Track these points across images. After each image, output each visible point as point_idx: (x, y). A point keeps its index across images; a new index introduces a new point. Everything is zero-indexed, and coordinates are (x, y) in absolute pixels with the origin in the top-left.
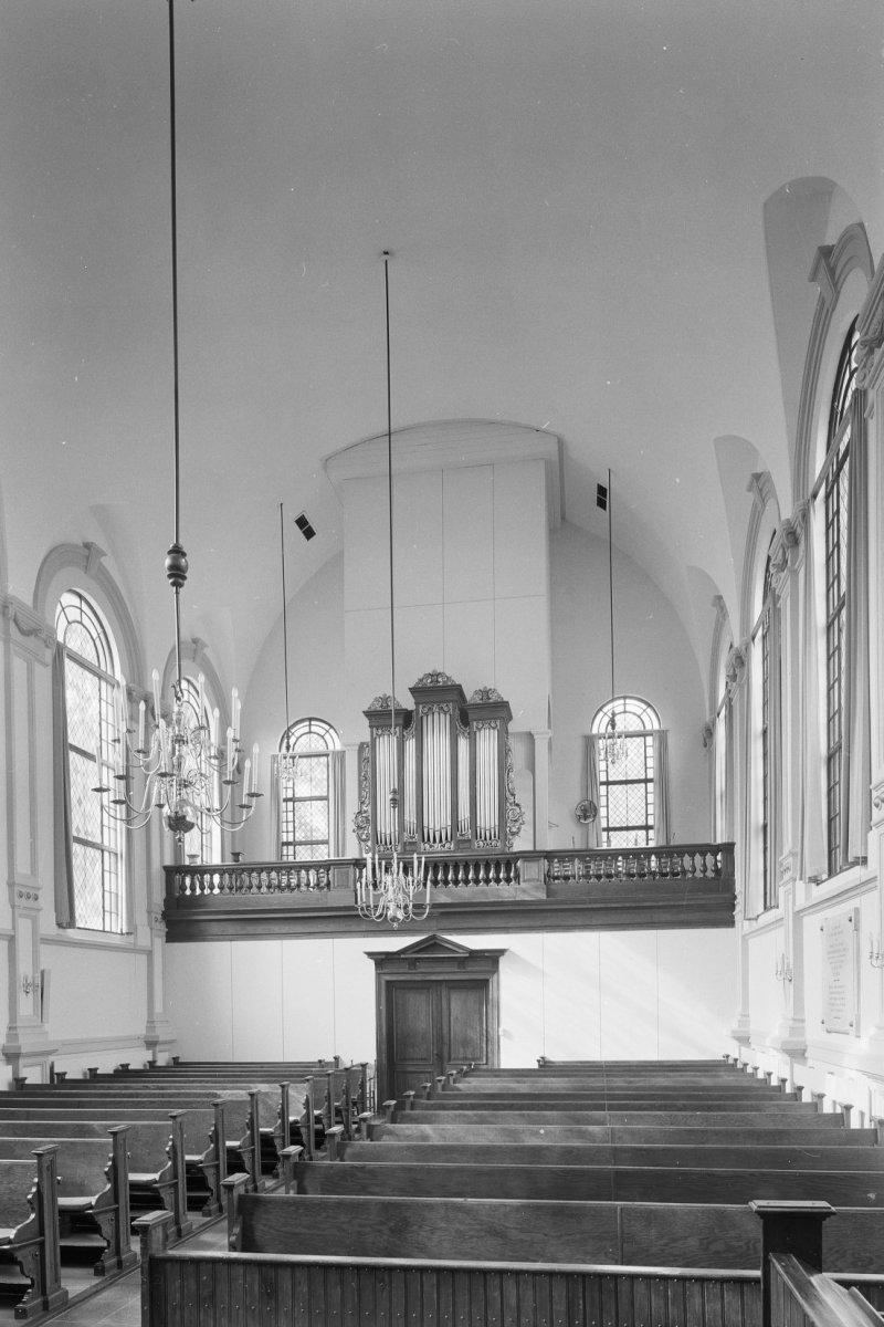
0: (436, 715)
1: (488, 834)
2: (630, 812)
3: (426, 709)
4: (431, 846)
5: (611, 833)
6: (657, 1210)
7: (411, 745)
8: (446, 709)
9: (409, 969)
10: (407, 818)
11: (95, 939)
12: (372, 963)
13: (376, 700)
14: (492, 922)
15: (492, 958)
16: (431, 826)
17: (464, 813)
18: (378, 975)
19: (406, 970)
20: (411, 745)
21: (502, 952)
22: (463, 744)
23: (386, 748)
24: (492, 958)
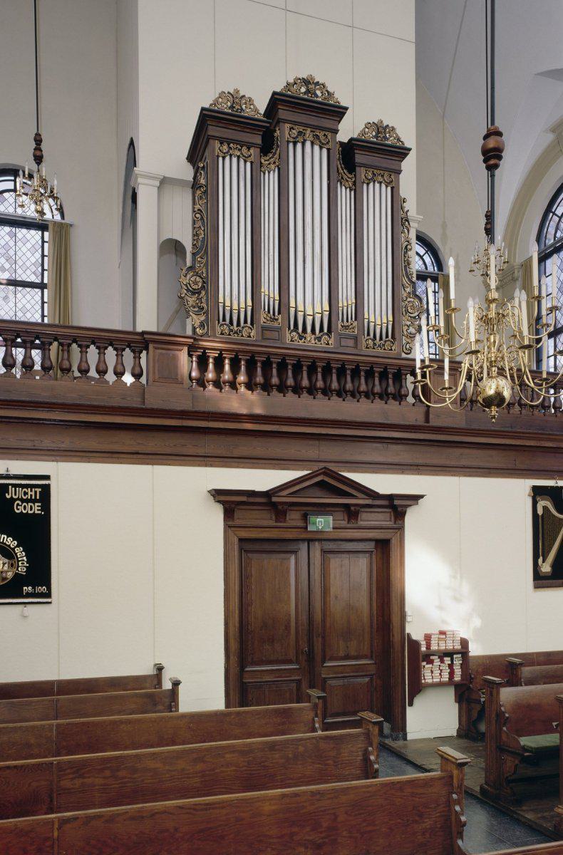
0: (308, 144)
1: (309, 319)
2: (20, 244)
3: (295, 132)
4: (301, 337)
5: (38, 281)
6: (287, 793)
7: (271, 181)
8: (322, 138)
9: (349, 522)
10: (264, 289)
11: (282, 536)
12: (216, 515)
13: (368, 125)
14: (453, 456)
15: (397, 507)
16: (301, 308)
17: (270, 287)
18: (227, 527)
19: (272, 523)
20: (271, 181)
21: (416, 498)
22: (344, 195)
23: (232, 174)
24: (397, 507)
